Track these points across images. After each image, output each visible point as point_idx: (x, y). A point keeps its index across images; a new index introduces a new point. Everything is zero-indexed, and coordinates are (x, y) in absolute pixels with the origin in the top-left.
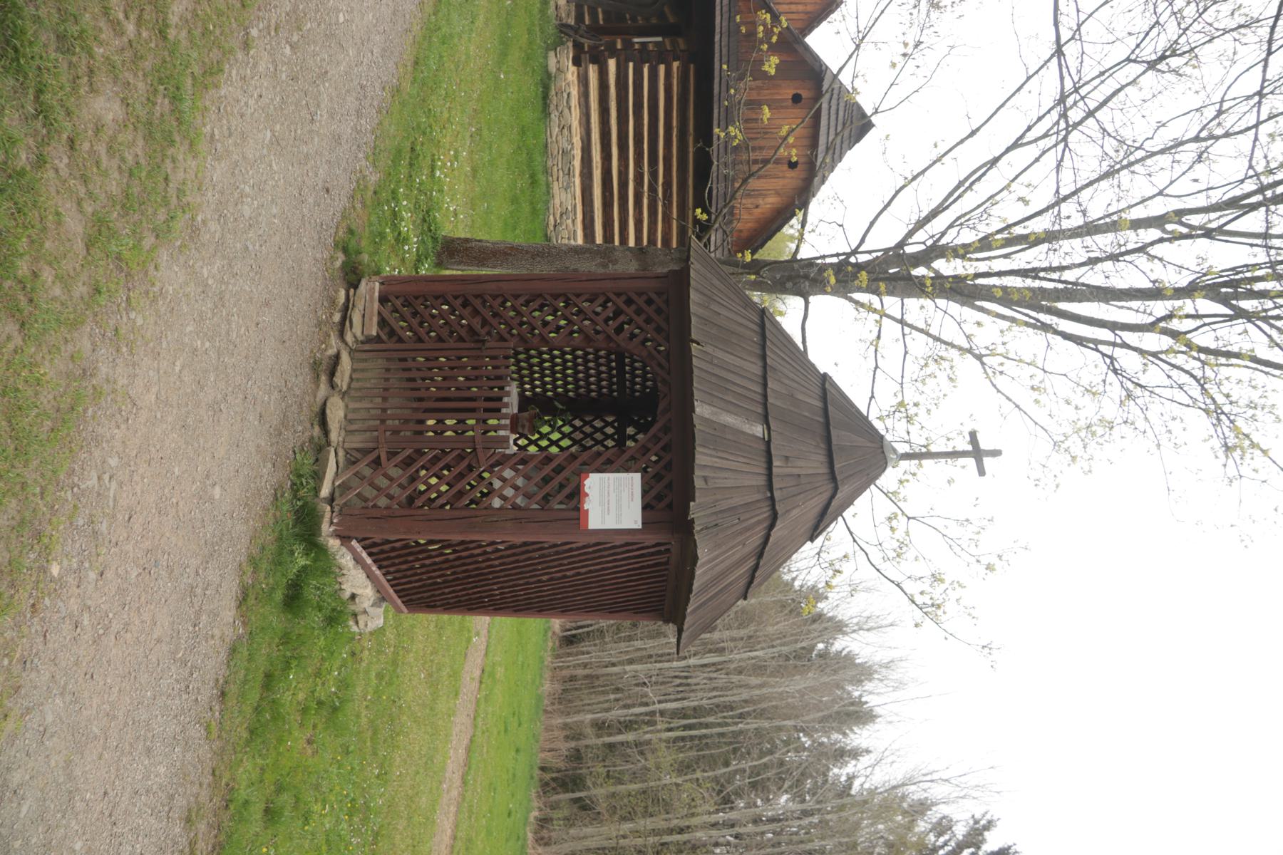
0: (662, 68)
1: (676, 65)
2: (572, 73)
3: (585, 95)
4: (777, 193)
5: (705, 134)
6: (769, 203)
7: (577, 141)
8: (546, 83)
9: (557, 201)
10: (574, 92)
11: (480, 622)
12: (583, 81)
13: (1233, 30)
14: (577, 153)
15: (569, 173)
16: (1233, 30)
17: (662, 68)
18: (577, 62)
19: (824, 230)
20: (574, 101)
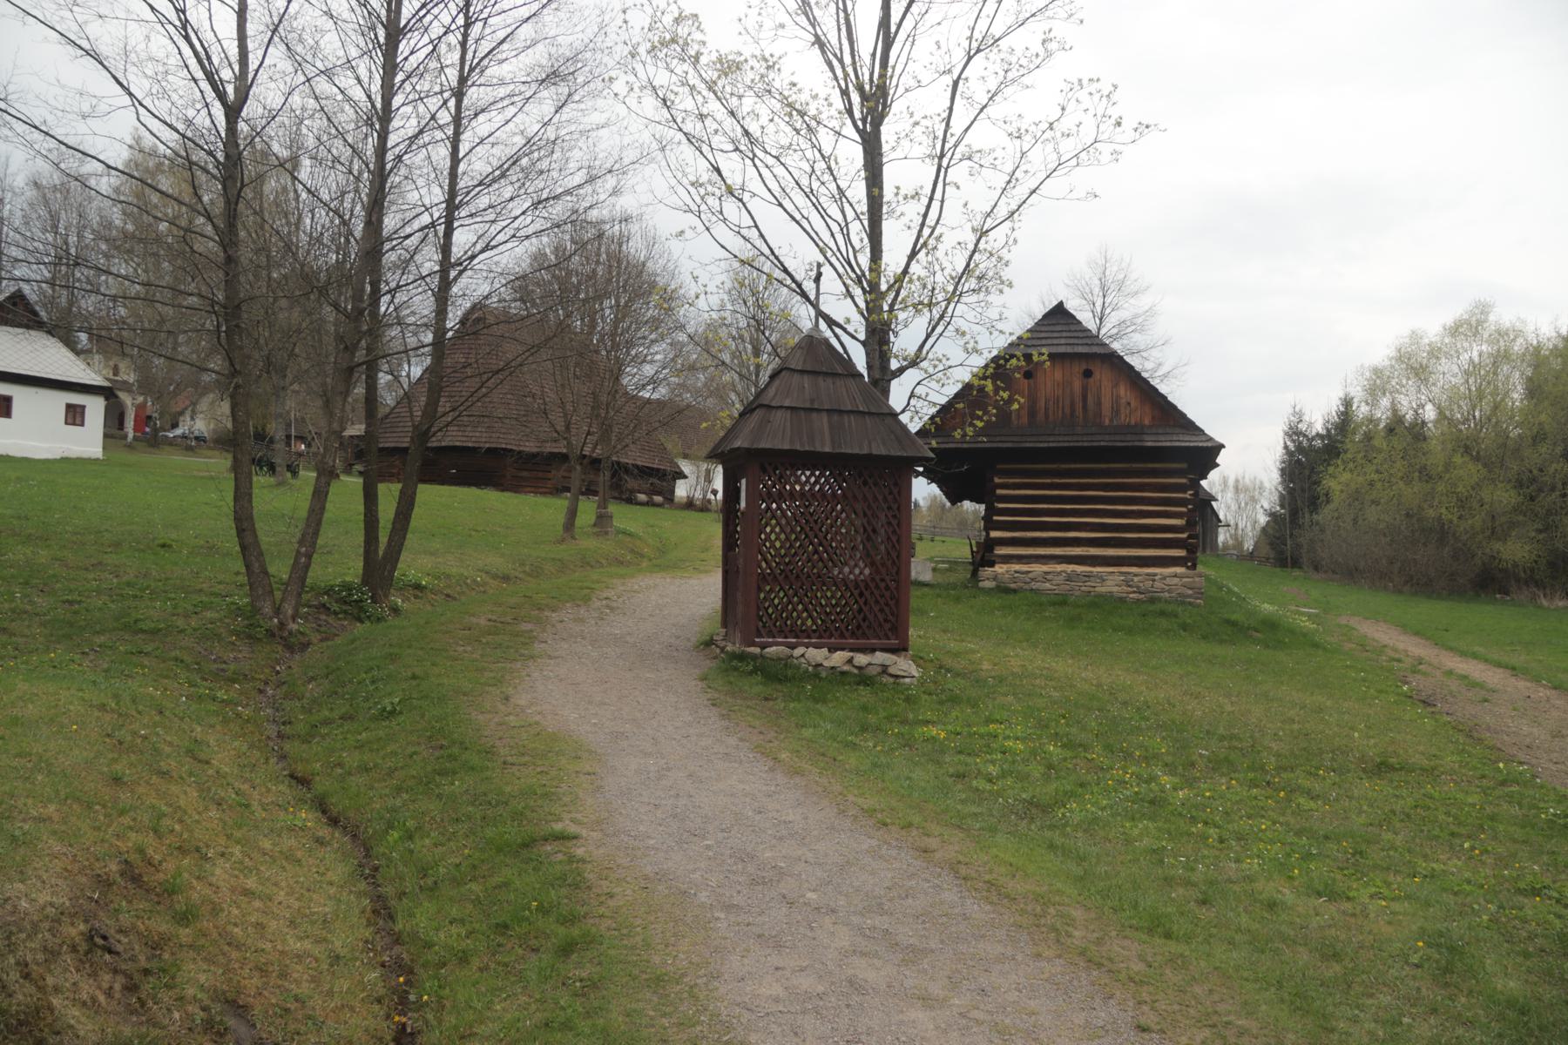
0: (999, 492)
1: (997, 480)
2: (999, 569)
3: (1020, 559)
4: (1116, 385)
5: (734, 427)
6: (1124, 392)
7: (1059, 568)
8: (1003, 589)
9: (1115, 589)
10: (1017, 567)
11: (402, 558)
12: (1007, 559)
13: (388, 91)
14: (1070, 568)
15: (1088, 576)
16: (388, 91)
17: (999, 492)
18: (992, 564)
19: (1094, 331)
20: (1025, 568)
